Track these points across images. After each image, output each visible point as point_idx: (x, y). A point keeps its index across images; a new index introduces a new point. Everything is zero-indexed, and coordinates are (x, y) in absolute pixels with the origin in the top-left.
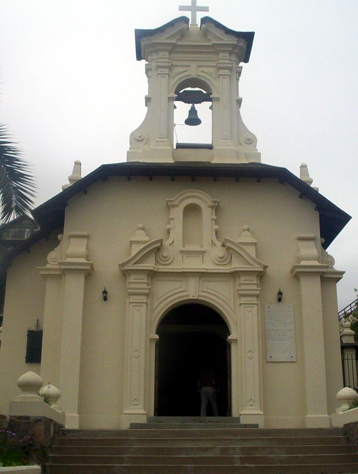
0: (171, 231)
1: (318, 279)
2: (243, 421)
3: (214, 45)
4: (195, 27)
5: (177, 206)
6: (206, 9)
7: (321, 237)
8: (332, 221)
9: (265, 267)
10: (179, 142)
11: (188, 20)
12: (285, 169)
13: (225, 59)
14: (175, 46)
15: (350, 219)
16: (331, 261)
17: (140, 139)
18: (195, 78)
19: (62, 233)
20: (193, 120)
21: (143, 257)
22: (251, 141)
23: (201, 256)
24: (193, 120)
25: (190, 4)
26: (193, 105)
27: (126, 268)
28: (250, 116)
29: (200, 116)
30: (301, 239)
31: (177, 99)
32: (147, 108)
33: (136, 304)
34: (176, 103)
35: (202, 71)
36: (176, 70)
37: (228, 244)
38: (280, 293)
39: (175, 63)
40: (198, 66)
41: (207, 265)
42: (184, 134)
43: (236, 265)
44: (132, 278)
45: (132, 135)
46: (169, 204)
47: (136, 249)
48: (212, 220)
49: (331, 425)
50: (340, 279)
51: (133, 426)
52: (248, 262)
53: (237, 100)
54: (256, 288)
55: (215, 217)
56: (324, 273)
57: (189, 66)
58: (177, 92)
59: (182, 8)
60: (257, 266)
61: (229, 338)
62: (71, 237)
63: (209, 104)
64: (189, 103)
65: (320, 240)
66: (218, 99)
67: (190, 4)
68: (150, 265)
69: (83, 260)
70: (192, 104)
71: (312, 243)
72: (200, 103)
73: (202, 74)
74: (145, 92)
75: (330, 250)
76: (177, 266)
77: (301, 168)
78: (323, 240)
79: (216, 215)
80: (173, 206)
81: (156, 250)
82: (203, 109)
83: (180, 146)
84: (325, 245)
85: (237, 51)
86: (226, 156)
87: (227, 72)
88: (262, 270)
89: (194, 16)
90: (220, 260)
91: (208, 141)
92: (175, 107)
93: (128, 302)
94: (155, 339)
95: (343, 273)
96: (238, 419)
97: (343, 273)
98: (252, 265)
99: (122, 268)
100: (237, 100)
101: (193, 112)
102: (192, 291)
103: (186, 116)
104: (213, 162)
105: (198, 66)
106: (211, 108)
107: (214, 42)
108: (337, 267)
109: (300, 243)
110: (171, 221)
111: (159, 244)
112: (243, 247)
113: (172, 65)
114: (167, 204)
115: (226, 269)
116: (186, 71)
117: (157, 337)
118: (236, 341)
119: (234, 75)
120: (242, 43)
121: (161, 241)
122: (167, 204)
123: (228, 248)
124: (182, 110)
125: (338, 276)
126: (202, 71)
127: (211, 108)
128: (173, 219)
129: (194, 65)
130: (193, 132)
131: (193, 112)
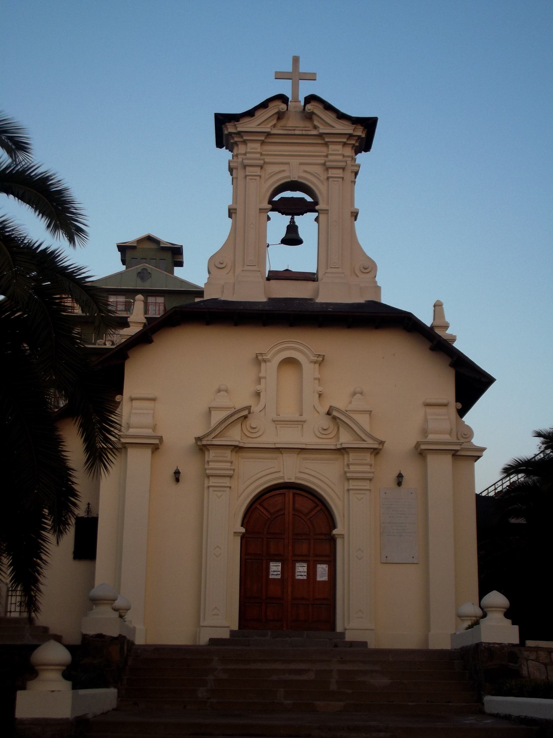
0: (261, 394)
1: (448, 458)
2: (349, 637)
3: (321, 136)
4: (297, 104)
5: (269, 361)
6: (312, 77)
7: (457, 401)
8: (471, 383)
9: (382, 443)
10: (272, 269)
11: (288, 99)
12: (410, 314)
13: (338, 152)
14: (268, 134)
15: (75, 553)
16: (468, 433)
17: (221, 266)
18: (296, 181)
19: (122, 394)
20: (292, 238)
21: (229, 422)
22: (369, 268)
23: (300, 426)
24: (292, 238)
25: (290, 69)
26: (292, 219)
27: (204, 442)
28: (369, 235)
29: (302, 234)
30: (428, 405)
31: (272, 210)
32: (230, 220)
33: (218, 489)
34: (271, 214)
35: (305, 171)
36: (270, 169)
37: (335, 413)
38: (400, 476)
39: (268, 159)
40: (301, 164)
41: (307, 438)
42: (280, 258)
43: (345, 439)
44: (212, 454)
45: (212, 260)
46: (259, 358)
47: (217, 417)
48: (315, 379)
49: (547, 677)
50: (479, 457)
51: (213, 642)
52: (361, 437)
53: (352, 213)
54: (369, 470)
55: (317, 375)
56: (457, 451)
57: (288, 164)
58: (270, 202)
59: (280, 76)
60: (369, 441)
61: (335, 532)
62: (132, 399)
63: (316, 214)
64: (287, 214)
65: (454, 406)
66: (326, 211)
67: (290, 69)
68: (235, 436)
69: (149, 432)
70: (291, 216)
71: (443, 410)
72: (302, 215)
73: (304, 175)
74: (229, 202)
75: (468, 419)
76: (269, 438)
77: (435, 306)
78: (460, 406)
79: (319, 374)
80: (265, 361)
81: (243, 416)
82: (306, 223)
83: (274, 276)
84: (462, 412)
85: (353, 142)
86: (330, 294)
87: (339, 173)
88: (376, 446)
89: (295, 89)
90: (323, 432)
91: (312, 268)
92: (269, 219)
93: (206, 485)
94: (240, 533)
95: (483, 449)
96: (342, 634)
97: (483, 449)
98: (365, 441)
99: (199, 443)
100: (352, 213)
101: (292, 228)
102: (290, 471)
103: (283, 234)
104: (319, 300)
105: (301, 164)
106: (317, 220)
107: (321, 131)
108: (476, 441)
109: (429, 410)
110: (263, 381)
111: (245, 413)
112: (351, 415)
113: (265, 163)
114: (257, 357)
115: (330, 444)
116: (284, 171)
117: (243, 530)
118: (342, 536)
119: (348, 176)
120: (360, 132)
121: (249, 408)
122: (257, 357)
123: (335, 418)
124: (278, 223)
125: (476, 454)
126: (305, 171)
127: (317, 220)
128: (265, 378)
129: (294, 162)
130: (294, 255)
131: (292, 228)
